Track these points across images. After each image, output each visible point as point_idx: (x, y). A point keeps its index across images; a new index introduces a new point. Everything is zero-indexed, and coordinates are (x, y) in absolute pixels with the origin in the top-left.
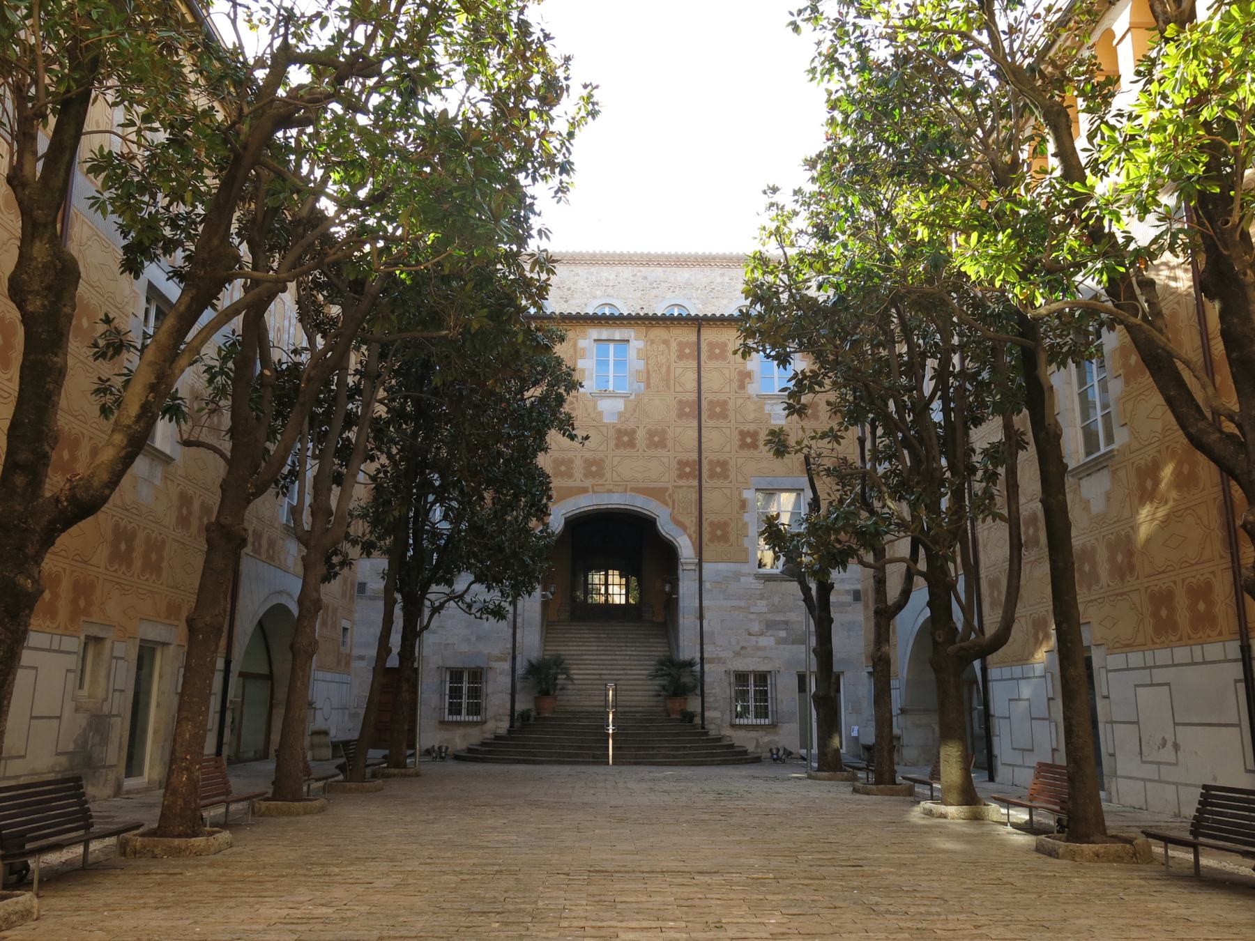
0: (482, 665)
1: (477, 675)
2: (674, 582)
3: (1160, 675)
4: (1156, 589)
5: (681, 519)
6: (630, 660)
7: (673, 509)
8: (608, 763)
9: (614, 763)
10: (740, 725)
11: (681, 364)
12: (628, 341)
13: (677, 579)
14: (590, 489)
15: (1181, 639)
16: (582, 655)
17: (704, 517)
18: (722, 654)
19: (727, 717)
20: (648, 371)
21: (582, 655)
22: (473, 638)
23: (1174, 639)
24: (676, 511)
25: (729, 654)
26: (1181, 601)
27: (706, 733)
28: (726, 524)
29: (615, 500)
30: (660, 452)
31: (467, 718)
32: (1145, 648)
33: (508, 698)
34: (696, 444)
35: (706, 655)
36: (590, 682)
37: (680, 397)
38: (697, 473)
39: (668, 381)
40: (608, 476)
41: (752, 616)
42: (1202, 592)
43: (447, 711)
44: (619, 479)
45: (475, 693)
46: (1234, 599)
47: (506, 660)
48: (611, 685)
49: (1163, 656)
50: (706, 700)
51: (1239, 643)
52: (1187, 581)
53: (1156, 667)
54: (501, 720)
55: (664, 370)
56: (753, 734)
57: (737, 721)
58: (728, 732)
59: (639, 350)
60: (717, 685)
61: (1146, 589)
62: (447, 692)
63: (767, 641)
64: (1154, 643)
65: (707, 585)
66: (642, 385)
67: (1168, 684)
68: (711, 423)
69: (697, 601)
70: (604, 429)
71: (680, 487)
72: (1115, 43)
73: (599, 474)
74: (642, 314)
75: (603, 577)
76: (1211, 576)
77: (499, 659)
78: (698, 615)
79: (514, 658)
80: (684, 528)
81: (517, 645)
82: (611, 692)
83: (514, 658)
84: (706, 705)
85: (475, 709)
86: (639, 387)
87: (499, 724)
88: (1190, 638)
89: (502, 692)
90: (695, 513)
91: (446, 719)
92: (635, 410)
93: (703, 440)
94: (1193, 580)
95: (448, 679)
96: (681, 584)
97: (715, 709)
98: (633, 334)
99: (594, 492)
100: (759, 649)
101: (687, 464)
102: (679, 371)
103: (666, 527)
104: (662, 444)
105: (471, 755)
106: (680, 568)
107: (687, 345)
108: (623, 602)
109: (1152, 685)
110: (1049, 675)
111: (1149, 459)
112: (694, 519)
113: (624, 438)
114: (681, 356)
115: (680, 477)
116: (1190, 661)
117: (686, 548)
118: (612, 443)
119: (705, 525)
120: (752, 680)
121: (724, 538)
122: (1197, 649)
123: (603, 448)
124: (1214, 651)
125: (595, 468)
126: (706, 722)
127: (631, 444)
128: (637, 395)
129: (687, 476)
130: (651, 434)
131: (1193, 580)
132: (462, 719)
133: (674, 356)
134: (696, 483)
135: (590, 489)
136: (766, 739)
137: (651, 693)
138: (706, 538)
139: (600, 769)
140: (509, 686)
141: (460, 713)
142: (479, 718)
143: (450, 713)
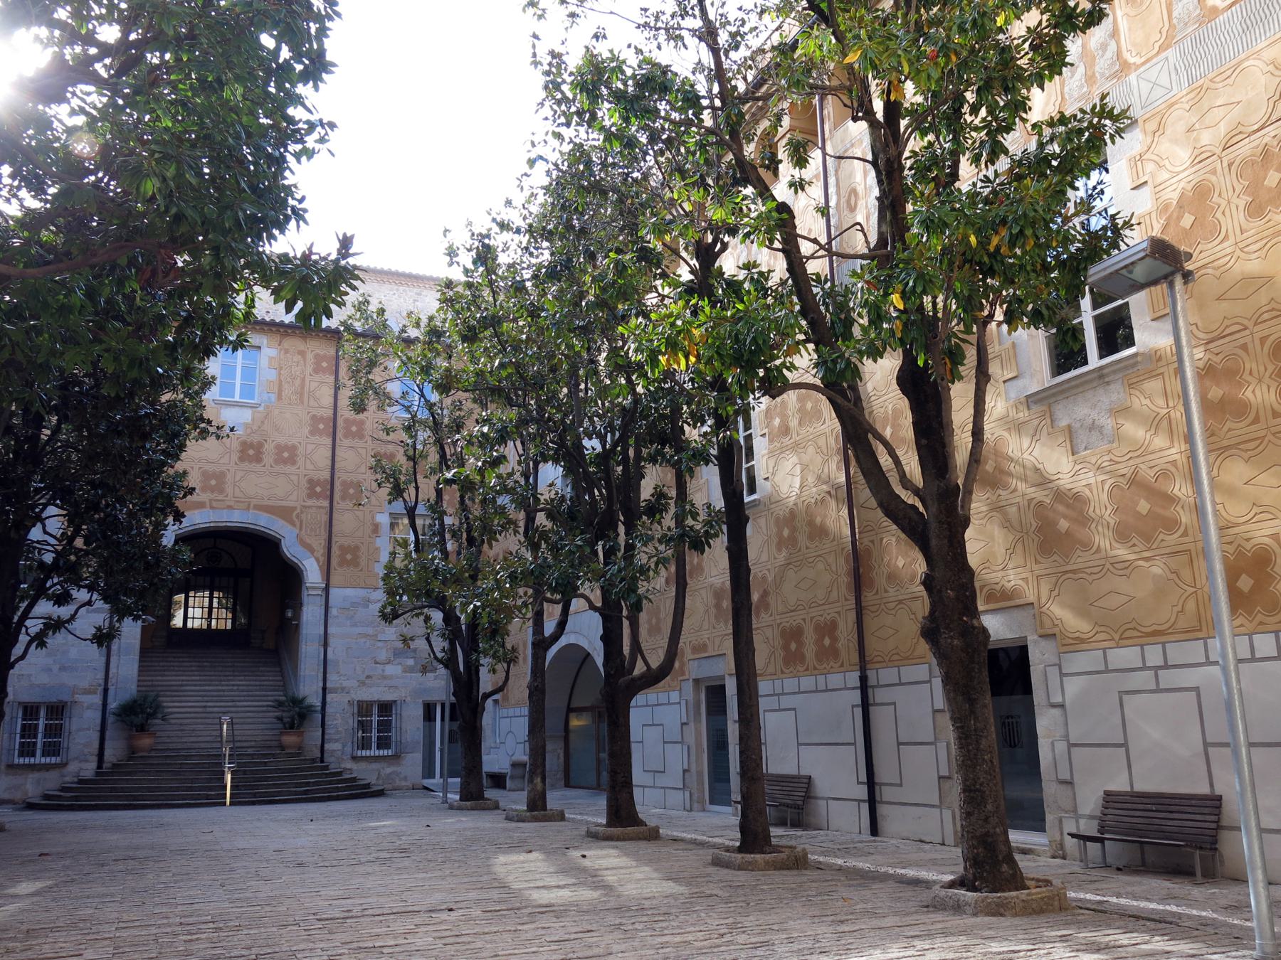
0: (65, 698)
1: (58, 710)
2: (298, 606)
3: (786, 701)
4: (788, 625)
5: (309, 541)
6: (238, 690)
7: (301, 529)
8: (224, 804)
9: (231, 804)
10: (362, 757)
11: (317, 377)
12: (260, 347)
13: (301, 605)
14: (208, 504)
15: (807, 670)
16: (182, 685)
17: (334, 539)
18: (345, 684)
19: (348, 749)
20: (280, 381)
21: (182, 685)
22: (55, 668)
23: (801, 669)
24: (303, 532)
25: (353, 683)
26: (809, 637)
27: (326, 768)
28: (357, 548)
29: (235, 518)
30: (289, 469)
31: (43, 760)
32: (775, 677)
33: (95, 736)
34: (329, 463)
35: (328, 685)
36: (192, 715)
37: (314, 412)
38: (328, 493)
39: (301, 395)
40: (229, 490)
41: (380, 644)
42: (828, 629)
43: (17, 752)
44: (242, 495)
45: (54, 731)
46: (856, 636)
47: (96, 693)
48: (226, 719)
49: (790, 684)
50: (326, 732)
51: (858, 673)
52: (814, 620)
53: (783, 694)
54: (87, 761)
55: (298, 382)
56: (375, 766)
57: (359, 753)
58: (349, 765)
59: (271, 358)
60: (341, 719)
61: (779, 625)
62: (18, 730)
63: (393, 670)
64: (782, 672)
65: (334, 612)
66: (273, 397)
67: (794, 709)
68: (347, 442)
69: (322, 628)
71: (309, 507)
72: (776, 140)
73: (220, 489)
74: (268, 319)
75: (207, 600)
76: (836, 615)
77: (87, 692)
78: (322, 643)
79: (106, 691)
80: (312, 551)
81: (111, 675)
82: (225, 726)
83: (106, 691)
84: (326, 737)
85: (52, 749)
86: (269, 398)
87: (85, 765)
88: (815, 668)
89: (89, 729)
90: (324, 535)
91: (16, 761)
92: (263, 422)
93: (337, 459)
94: (820, 618)
95: (20, 715)
96: (305, 609)
97: (336, 741)
98: (265, 341)
99: (212, 507)
100: (384, 677)
101: (318, 483)
102: (314, 385)
103: (291, 549)
104: (292, 460)
105: (50, 803)
106: (305, 593)
107: (324, 358)
108: (229, 626)
109: (779, 710)
110: (683, 703)
111: (787, 510)
112: (323, 542)
113: (251, 452)
114: (317, 370)
115: (310, 496)
116: (1154, 687)
117: (312, 574)
118: (235, 457)
119: (335, 550)
120: (42, 713)
121: (355, 563)
122: (821, 679)
123: (225, 460)
124: (835, 680)
125: (216, 481)
126: (325, 755)
127: (258, 458)
128: (267, 407)
129: (318, 496)
130: (280, 448)
131: (820, 618)
132: (37, 762)
133: (309, 369)
134: (326, 504)
135: (208, 504)
136: (389, 770)
137: (263, 726)
138: (334, 562)
139: (212, 812)
140: (98, 721)
141: (34, 755)
142: (59, 759)
143: (21, 754)
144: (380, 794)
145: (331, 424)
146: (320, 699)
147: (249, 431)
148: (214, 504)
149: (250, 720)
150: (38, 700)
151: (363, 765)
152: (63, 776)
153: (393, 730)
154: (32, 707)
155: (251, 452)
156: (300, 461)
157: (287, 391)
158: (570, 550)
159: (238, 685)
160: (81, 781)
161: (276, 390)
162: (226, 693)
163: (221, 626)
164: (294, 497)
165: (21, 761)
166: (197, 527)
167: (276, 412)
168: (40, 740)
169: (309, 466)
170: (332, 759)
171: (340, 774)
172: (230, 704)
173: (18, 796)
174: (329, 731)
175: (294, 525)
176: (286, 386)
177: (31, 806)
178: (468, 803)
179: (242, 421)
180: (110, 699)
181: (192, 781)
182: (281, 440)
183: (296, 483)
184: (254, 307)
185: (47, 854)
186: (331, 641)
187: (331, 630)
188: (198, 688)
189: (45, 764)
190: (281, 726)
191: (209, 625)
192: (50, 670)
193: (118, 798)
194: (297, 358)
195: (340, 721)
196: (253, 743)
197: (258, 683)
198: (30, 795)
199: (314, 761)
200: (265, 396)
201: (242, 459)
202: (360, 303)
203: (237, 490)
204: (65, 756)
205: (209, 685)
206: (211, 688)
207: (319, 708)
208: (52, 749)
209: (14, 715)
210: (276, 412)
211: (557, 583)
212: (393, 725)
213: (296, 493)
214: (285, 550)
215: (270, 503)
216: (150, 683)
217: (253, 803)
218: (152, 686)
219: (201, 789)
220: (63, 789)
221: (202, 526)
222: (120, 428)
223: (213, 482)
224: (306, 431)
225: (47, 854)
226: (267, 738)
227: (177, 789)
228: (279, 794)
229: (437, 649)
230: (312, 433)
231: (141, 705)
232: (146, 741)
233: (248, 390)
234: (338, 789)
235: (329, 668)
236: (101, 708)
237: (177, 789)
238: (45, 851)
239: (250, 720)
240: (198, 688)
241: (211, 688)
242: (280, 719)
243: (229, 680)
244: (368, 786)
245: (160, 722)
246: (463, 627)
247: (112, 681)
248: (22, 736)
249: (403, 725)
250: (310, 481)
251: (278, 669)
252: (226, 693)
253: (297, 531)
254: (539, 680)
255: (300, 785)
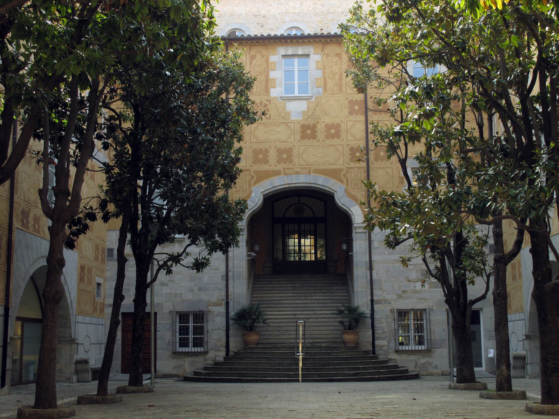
0: (204, 309)
1: (200, 317)
5: (353, 193)
6: (318, 303)
7: (347, 185)
10: (402, 351)
12: (309, 55)
14: (282, 172)
18: (387, 297)
22: (196, 289)
24: (349, 187)
27: (376, 357)
30: (335, 141)
31: (193, 350)
33: (224, 334)
35: (375, 298)
40: (296, 160)
43: (178, 344)
45: (199, 330)
47: (221, 305)
50: (376, 332)
54: (219, 350)
55: (337, 77)
56: (413, 357)
58: (394, 356)
59: (317, 62)
62: (178, 330)
66: (321, 90)
69: (368, 256)
70: (292, 125)
71: (352, 168)
73: (289, 160)
77: (217, 304)
78: (368, 267)
79: (227, 303)
81: (230, 293)
83: (227, 303)
84: (376, 336)
86: (318, 91)
89: (219, 329)
91: (178, 350)
92: (315, 110)
95: (178, 320)
96: (354, 243)
97: (383, 339)
98: (312, 50)
99: (285, 174)
103: (342, 200)
104: (337, 135)
106: (354, 231)
112: (364, 193)
118: (298, 137)
120: (191, 319)
126: (376, 349)
128: (317, 98)
130: (328, 127)
132: (190, 350)
135: (282, 172)
140: (224, 324)
143: (180, 346)
144: (416, 377)
145: (364, 105)
146: (370, 308)
147: (306, 117)
148: (287, 171)
149: (324, 324)
150: (187, 310)
151: (404, 357)
152: (206, 360)
153: (425, 331)
154: (184, 315)
155: (309, 132)
156: (343, 136)
157: (330, 84)
158: (484, 179)
159: (318, 300)
160: (216, 363)
161: (322, 85)
162: (310, 305)
163: (308, 259)
164: (341, 161)
165: (181, 349)
166: (277, 188)
167: (324, 101)
168: (191, 336)
169: (350, 138)
170: (381, 352)
171: (386, 362)
172: (312, 312)
173: (181, 372)
174: (378, 332)
175: (341, 181)
176: (329, 81)
177: (187, 379)
178: (462, 385)
179: (301, 110)
180: (231, 309)
181: (279, 364)
182: (328, 120)
183: (341, 151)
184: (213, 17)
185: (153, 406)
186: (375, 266)
187: (374, 258)
188: (291, 302)
189: (195, 352)
190: (342, 328)
191: (300, 258)
192: (192, 290)
193: (232, 375)
194: (336, 59)
195: (385, 325)
196: (325, 340)
197: (332, 298)
198: (188, 372)
199: (367, 352)
200: (315, 90)
201: (303, 138)
202: (355, 9)
203: (301, 160)
204: (205, 346)
205: (298, 300)
206: (300, 302)
207: (369, 315)
208: (198, 343)
209: (174, 320)
210: (324, 101)
211: (474, 206)
212: (425, 328)
213: (342, 158)
214: (337, 201)
215: (324, 167)
216: (260, 299)
217: (318, 381)
218: (261, 300)
219: (285, 370)
220: (206, 369)
221: (279, 188)
222: (158, 118)
223: (285, 156)
224: (346, 112)
225: (153, 406)
226: (334, 336)
227: (269, 369)
228: (337, 375)
229: (432, 267)
230: (351, 113)
231: (248, 313)
232: (253, 338)
233: (303, 88)
234: (380, 373)
235: (375, 286)
236: (225, 315)
237: (269, 369)
238: (151, 404)
239: (324, 324)
240: (291, 302)
241: (300, 302)
242: (342, 322)
243: (311, 296)
244: (406, 371)
245: (262, 325)
246: (452, 248)
247: (231, 297)
248: (180, 334)
249: (432, 328)
250: (352, 149)
251: (346, 288)
252: (310, 305)
253: (345, 186)
254: (501, 288)
255: (354, 369)
